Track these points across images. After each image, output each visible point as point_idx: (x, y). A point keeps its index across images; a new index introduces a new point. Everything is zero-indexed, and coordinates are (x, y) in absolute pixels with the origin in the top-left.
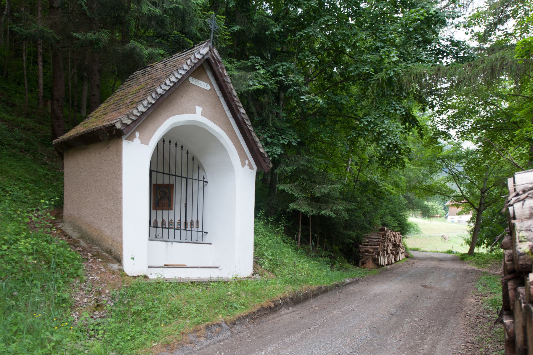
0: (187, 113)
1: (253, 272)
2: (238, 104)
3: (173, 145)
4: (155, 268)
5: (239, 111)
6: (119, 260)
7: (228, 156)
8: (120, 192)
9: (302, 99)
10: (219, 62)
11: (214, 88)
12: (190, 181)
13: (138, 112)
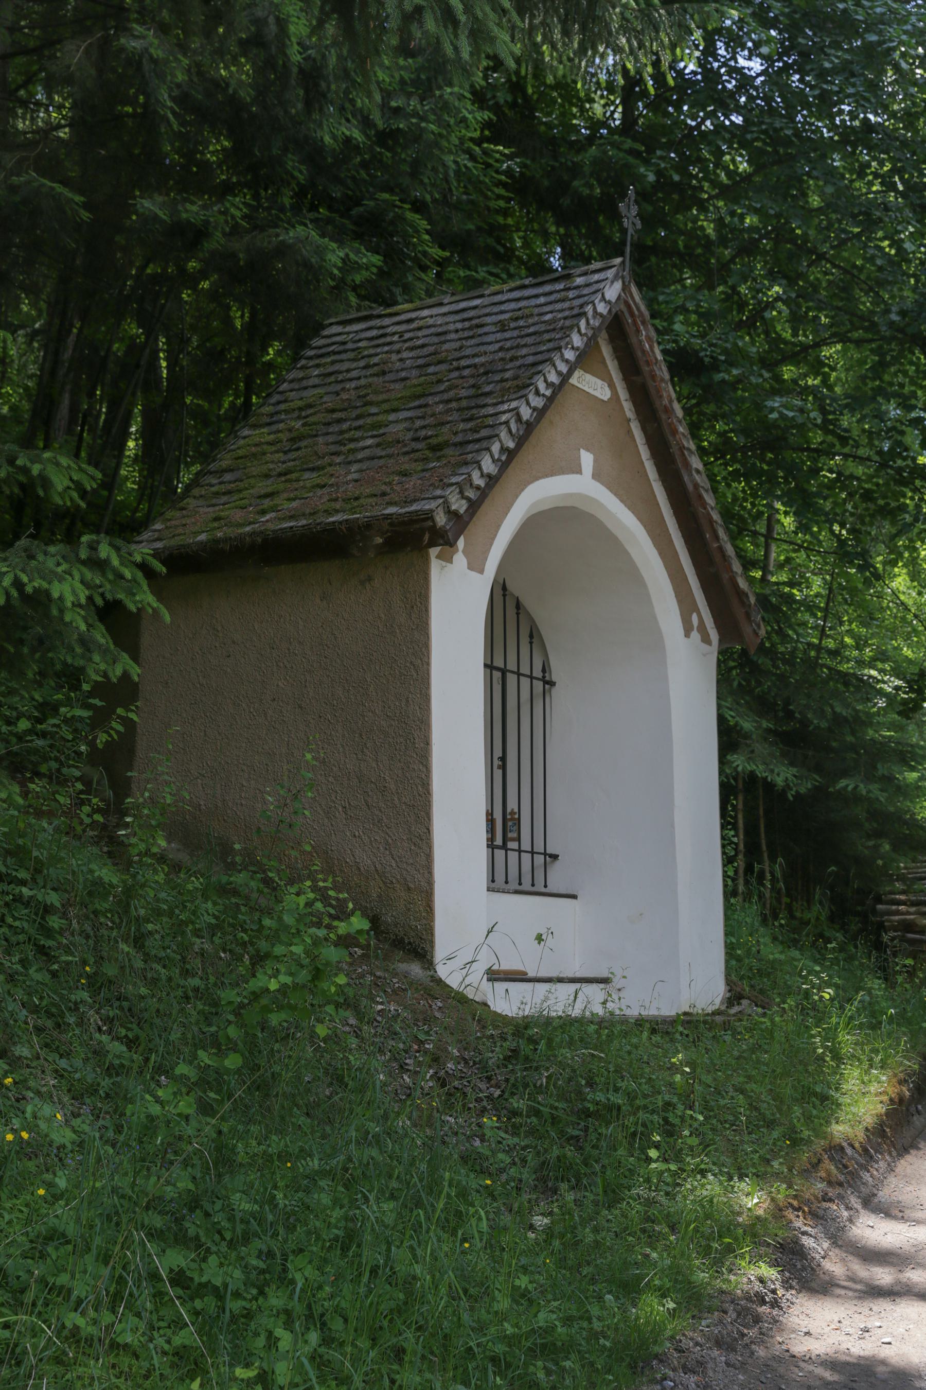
5: (687, 465)
8: (424, 723)
10: (643, 323)
12: (511, 679)
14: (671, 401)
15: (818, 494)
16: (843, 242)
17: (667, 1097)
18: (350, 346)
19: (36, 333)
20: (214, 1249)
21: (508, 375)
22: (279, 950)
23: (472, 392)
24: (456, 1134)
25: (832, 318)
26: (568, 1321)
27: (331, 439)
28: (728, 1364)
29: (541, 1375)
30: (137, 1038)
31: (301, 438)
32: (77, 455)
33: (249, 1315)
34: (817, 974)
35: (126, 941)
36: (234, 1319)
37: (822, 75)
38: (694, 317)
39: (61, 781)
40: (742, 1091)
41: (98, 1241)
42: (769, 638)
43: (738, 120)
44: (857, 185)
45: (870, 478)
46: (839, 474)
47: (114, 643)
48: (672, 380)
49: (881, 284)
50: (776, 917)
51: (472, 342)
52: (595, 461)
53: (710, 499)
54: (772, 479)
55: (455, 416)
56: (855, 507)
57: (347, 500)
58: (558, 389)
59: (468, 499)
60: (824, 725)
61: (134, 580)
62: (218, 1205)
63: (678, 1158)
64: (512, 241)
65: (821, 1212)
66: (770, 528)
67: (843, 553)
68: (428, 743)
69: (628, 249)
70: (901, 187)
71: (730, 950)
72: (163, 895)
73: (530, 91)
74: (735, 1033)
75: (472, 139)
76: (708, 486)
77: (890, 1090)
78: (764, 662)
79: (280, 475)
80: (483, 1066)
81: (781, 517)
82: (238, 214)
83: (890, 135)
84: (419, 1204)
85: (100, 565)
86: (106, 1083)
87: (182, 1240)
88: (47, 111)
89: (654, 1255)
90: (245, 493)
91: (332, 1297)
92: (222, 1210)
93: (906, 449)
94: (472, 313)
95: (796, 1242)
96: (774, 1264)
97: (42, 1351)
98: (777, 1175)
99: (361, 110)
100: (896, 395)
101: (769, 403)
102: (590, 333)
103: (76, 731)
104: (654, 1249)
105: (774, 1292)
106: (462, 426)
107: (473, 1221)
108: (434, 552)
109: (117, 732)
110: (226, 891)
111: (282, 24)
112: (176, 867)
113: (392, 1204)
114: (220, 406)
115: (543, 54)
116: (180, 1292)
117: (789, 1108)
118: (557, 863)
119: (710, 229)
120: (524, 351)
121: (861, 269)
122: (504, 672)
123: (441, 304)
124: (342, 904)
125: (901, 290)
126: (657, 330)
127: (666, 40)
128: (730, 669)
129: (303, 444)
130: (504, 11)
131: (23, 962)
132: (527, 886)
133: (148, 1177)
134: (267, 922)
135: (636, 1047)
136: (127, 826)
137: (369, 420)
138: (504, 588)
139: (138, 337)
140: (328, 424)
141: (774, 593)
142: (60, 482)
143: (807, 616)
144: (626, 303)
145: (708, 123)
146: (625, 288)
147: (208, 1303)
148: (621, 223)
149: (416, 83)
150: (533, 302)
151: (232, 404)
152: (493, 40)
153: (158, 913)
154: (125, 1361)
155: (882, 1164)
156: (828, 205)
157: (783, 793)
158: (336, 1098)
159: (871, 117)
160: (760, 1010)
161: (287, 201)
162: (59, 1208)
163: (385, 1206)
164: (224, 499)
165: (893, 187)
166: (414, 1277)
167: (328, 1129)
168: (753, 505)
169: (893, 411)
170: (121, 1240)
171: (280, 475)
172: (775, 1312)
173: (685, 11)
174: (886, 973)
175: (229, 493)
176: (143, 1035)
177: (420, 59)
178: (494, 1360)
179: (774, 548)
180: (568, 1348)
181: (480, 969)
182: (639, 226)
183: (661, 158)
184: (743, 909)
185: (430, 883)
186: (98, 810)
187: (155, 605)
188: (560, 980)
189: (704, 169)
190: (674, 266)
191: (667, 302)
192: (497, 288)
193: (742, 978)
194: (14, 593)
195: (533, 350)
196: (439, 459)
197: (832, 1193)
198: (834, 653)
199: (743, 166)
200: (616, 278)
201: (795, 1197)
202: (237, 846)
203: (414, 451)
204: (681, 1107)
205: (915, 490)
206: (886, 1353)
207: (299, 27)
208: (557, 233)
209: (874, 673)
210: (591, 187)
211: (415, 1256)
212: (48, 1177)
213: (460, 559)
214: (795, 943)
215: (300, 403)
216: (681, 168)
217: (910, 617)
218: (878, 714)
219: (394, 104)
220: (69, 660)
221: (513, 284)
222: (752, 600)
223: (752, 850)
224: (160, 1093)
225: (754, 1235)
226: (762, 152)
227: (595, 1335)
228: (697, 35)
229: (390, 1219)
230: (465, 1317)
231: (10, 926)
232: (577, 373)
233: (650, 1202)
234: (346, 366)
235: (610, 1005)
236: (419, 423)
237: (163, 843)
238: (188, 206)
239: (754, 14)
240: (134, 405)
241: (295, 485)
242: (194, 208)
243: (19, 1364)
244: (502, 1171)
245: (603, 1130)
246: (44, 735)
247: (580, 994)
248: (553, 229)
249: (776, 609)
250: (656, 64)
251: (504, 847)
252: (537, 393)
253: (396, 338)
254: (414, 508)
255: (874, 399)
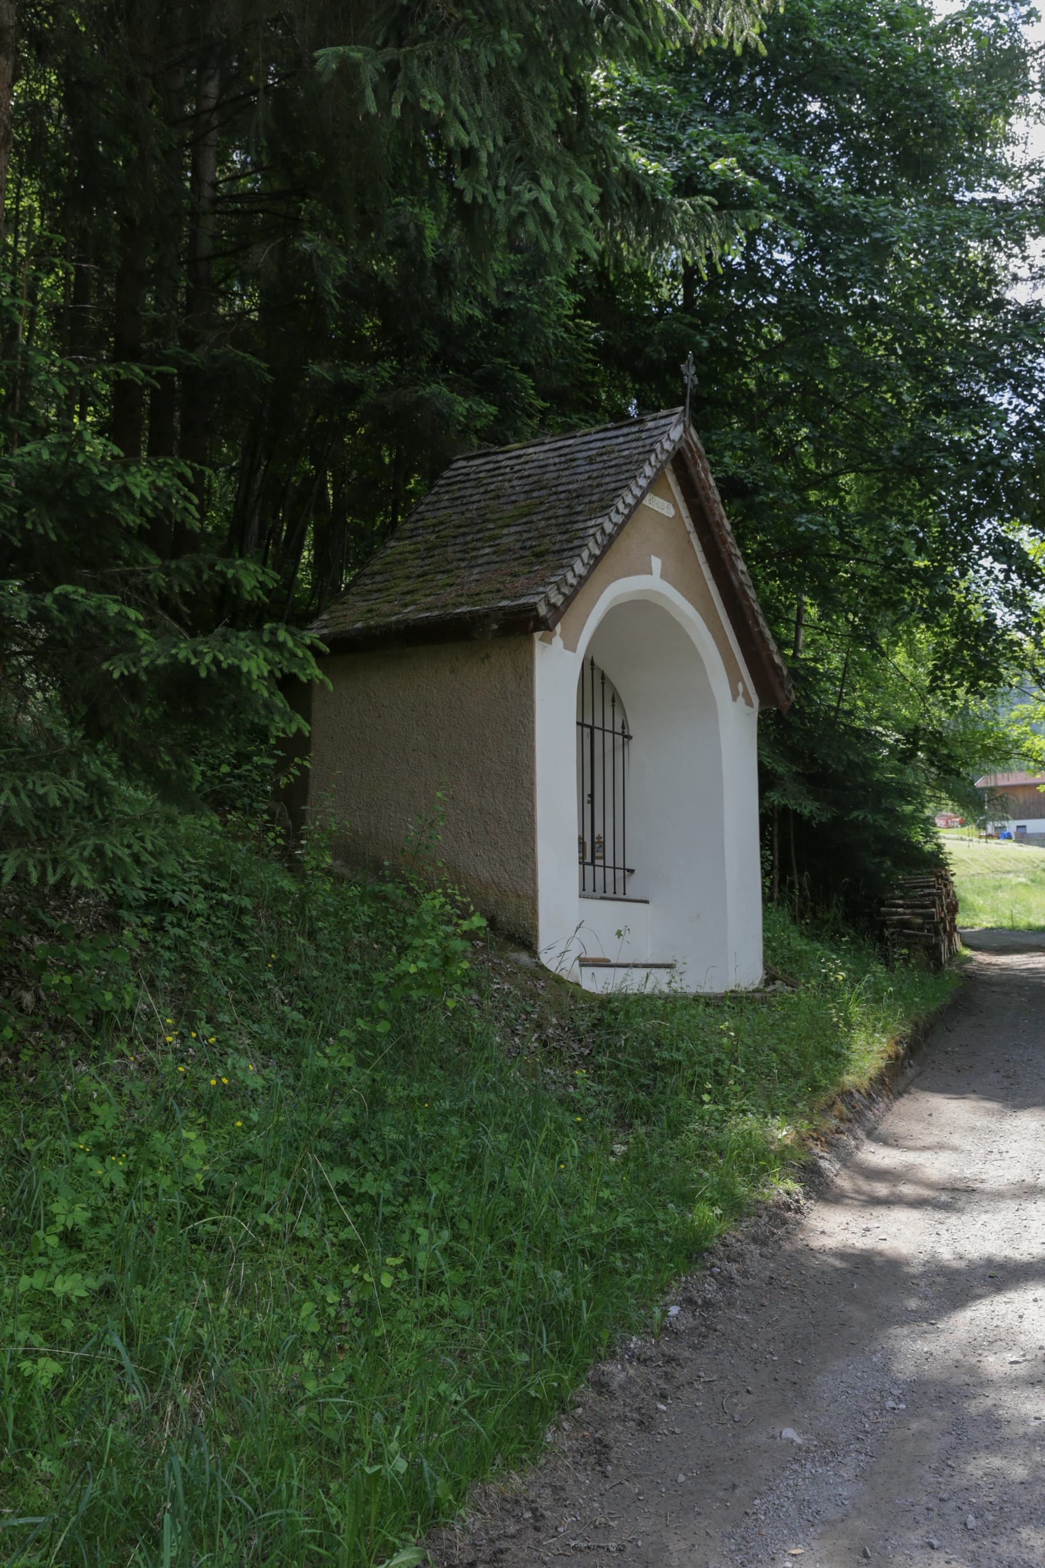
0: (629, 574)
5: (734, 567)
6: (527, 942)
8: (530, 768)
9: (801, 525)
10: (700, 457)
12: (598, 734)
14: (721, 517)
15: (837, 590)
16: (855, 395)
17: (717, 1055)
18: (473, 476)
19: (233, 469)
20: (370, 1168)
21: (594, 498)
22: (417, 942)
23: (567, 511)
24: (554, 1083)
25: (847, 453)
26: (640, 1223)
27: (457, 548)
28: (761, 1255)
29: (619, 1263)
30: (311, 1009)
31: (435, 547)
32: (264, 564)
33: (397, 1217)
34: (833, 961)
35: (302, 934)
36: (385, 1219)
37: (838, 265)
38: (739, 453)
39: (250, 812)
40: (775, 1051)
41: (282, 1160)
42: (798, 702)
43: (774, 300)
44: (866, 350)
45: (877, 577)
46: (853, 574)
47: (292, 708)
48: (722, 501)
49: (885, 427)
50: (802, 917)
51: (567, 472)
52: (663, 564)
53: (752, 594)
54: (801, 578)
55: (554, 530)
56: (865, 600)
57: (470, 596)
58: (633, 509)
59: (564, 594)
60: (841, 769)
61: (305, 658)
62: (373, 1135)
63: (725, 1101)
64: (599, 396)
65: (834, 1142)
66: (799, 616)
67: (857, 637)
68: (533, 783)
69: (688, 401)
70: (900, 352)
71: (767, 942)
72: (330, 900)
73: (612, 278)
74: (770, 1006)
75: (566, 316)
76: (750, 583)
77: (889, 1049)
78: (795, 720)
79: (419, 576)
80: (576, 1031)
81: (808, 608)
82: (386, 375)
83: (892, 312)
84: (526, 1136)
85: (278, 646)
86: (288, 1042)
87: (346, 1161)
88: (242, 300)
89: (706, 1174)
90: (392, 591)
91: (460, 1204)
92: (376, 1138)
93: (905, 555)
94: (567, 451)
95: (815, 1164)
96: (798, 1180)
97: (242, 1242)
98: (801, 1114)
99: (481, 295)
100: (895, 513)
101: (798, 520)
102: (658, 465)
103: (264, 775)
104: (706, 1169)
105: (797, 1201)
106: (559, 538)
107: (568, 1149)
108: (537, 635)
109: (294, 776)
110: (378, 897)
111: (420, 229)
112: (340, 879)
113: (505, 1135)
114: (374, 524)
115: (621, 250)
116: (344, 1199)
117: (811, 1063)
118: (634, 876)
119: (752, 384)
120: (608, 479)
121: (869, 415)
122: (592, 728)
123: (543, 444)
124: (466, 906)
125: (900, 431)
126: (711, 463)
127: (717, 239)
128: (768, 726)
129: (436, 552)
130: (591, 218)
131: (225, 951)
132: (610, 893)
133: (319, 1114)
134: (410, 921)
135: (694, 1017)
136: (302, 847)
137: (487, 534)
138: (592, 663)
139: (311, 471)
140: (456, 537)
141: (802, 667)
142: (249, 583)
143: (828, 684)
144: (687, 442)
145: (750, 303)
146: (685, 430)
147: (365, 1208)
148: (682, 380)
149: (524, 273)
150: (614, 441)
151: (383, 522)
152: (579, 238)
153: (327, 914)
154: (303, 1251)
155: (882, 1105)
156: (844, 366)
157: (809, 821)
158: (463, 1055)
159: (877, 298)
160: (789, 989)
161: (424, 365)
162: (253, 1136)
163: (500, 1137)
164: (376, 595)
165: (894, 352)
166: (523, 1190)
167: (457, 1078)
168: (786, 598)
169: (895, 526)
170: (299, 1160)
171: (419, 576)
172: (798, 1216)
173: (731, 216)
174: (887, 962)
175: (379, 590)
176: (315, 1007)
177: (526, 255)
178: (582, 1252)
179: (802, 631)
180: (640, 1243)
181: (575, 951)
182: (696, 382)
183: (713, 329)
184: (777, 911)
185: (535, 892)
186: (281, 836)
187: (321, 677)
188: (636, 966)
189: (747, 338)
190: (725, 413)
191: (718, 441)
192: (586, 430)
193: (776, 964)
194: (214, 668)
195: (614, 478)
196: (541, 563)
197: (843, 1127)
198: (849, 713)
199: (778, 336)
200: (678, 422)
201: (815, 1130)
202: (386, 863)
203: (522, 557)
204: (727, 1062)
205: (912, 587)
206: (882, 1246)
207: (432, 232)
208: (633, 388)
209: (879, 729)
210: (660, 352)
211: (523, 1175)
212: (245, 1113)
213: (558, 641)
214: (817, 937)
215: (434, 521)
216: (730, 337)
217: (907, 685)
218: (882, 760)
219: (506, 289)
220: (256, 720)
221: (598, 428)
222: (785, 672)
223: (785, 866)
224: (328, 1050)
225: (783, 1159)
226: (791, 325)
227: (660, 1234)
228: (741, 235)
229: (504, 1147)
230: (562, 1220)
231: (215, 924)
232: (648, 497)
233: (703, 1135)
234: (469, 492)
235: (673, 985)
236: (525, 536)
237: (329, 861)
238: (348, 370)
239: (785, 219)
240: (308, 523)
241: (430, 584)
242: (353, 371)
243: (224, 1251)
244: (589, 1110)
245: (668, 1080)
246: (239, 777)
247: (651, 977)
248: (630, 385)
249: (804, 679)
250: (709, 257)
251: (592, 863)
252: (618, 512)
253: (508, 470)
254: (522, 601)
255: (879, 517)
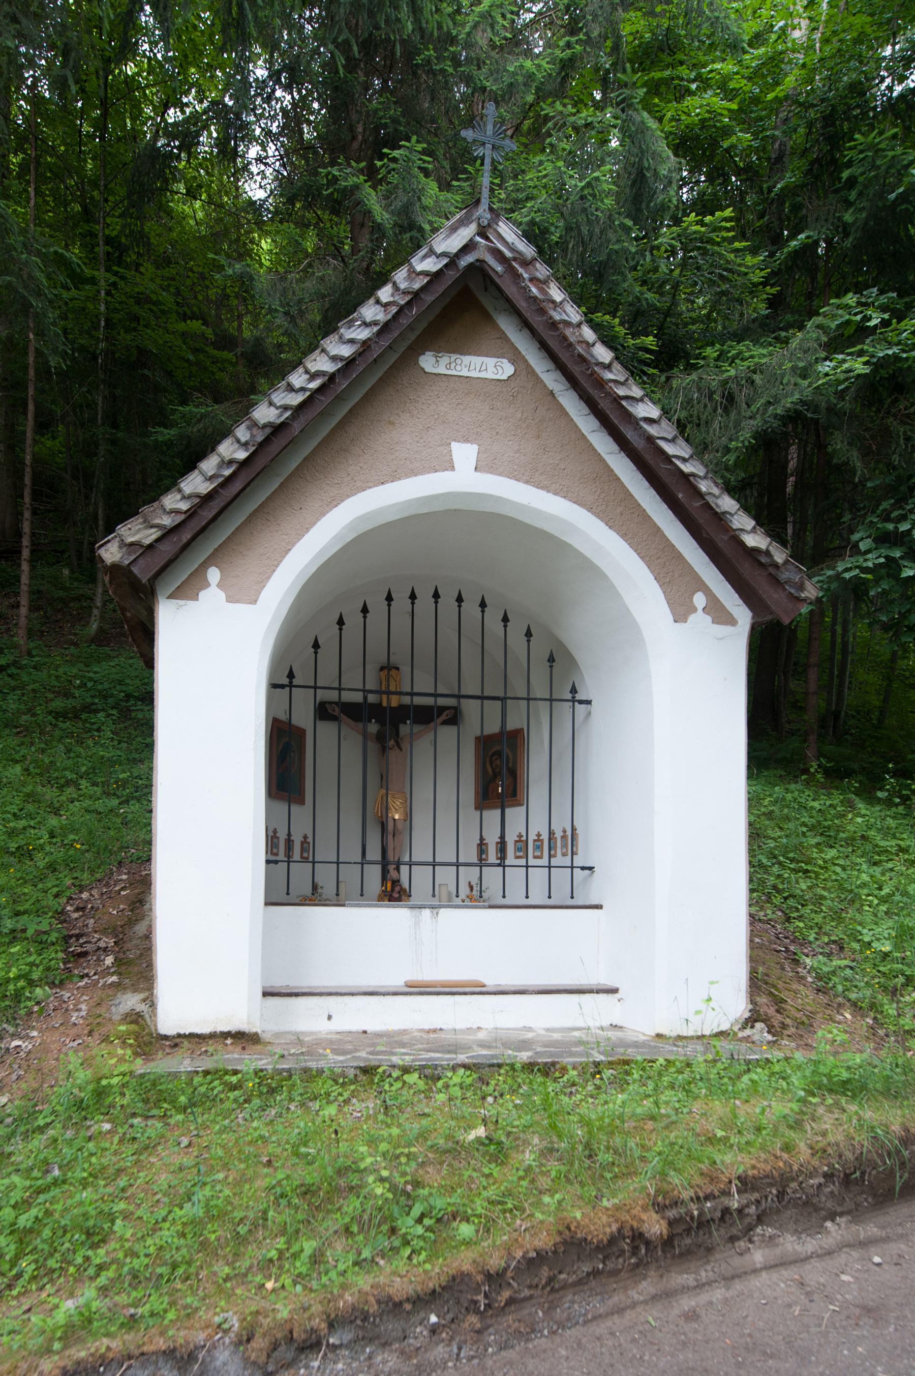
0: (414, 473)
1: (747, 1015)
2: (621, 392)
3: (471, 608)
4: (346, 998)
7: (618, 595)
11: (528, 366)
13: (184, 498)
